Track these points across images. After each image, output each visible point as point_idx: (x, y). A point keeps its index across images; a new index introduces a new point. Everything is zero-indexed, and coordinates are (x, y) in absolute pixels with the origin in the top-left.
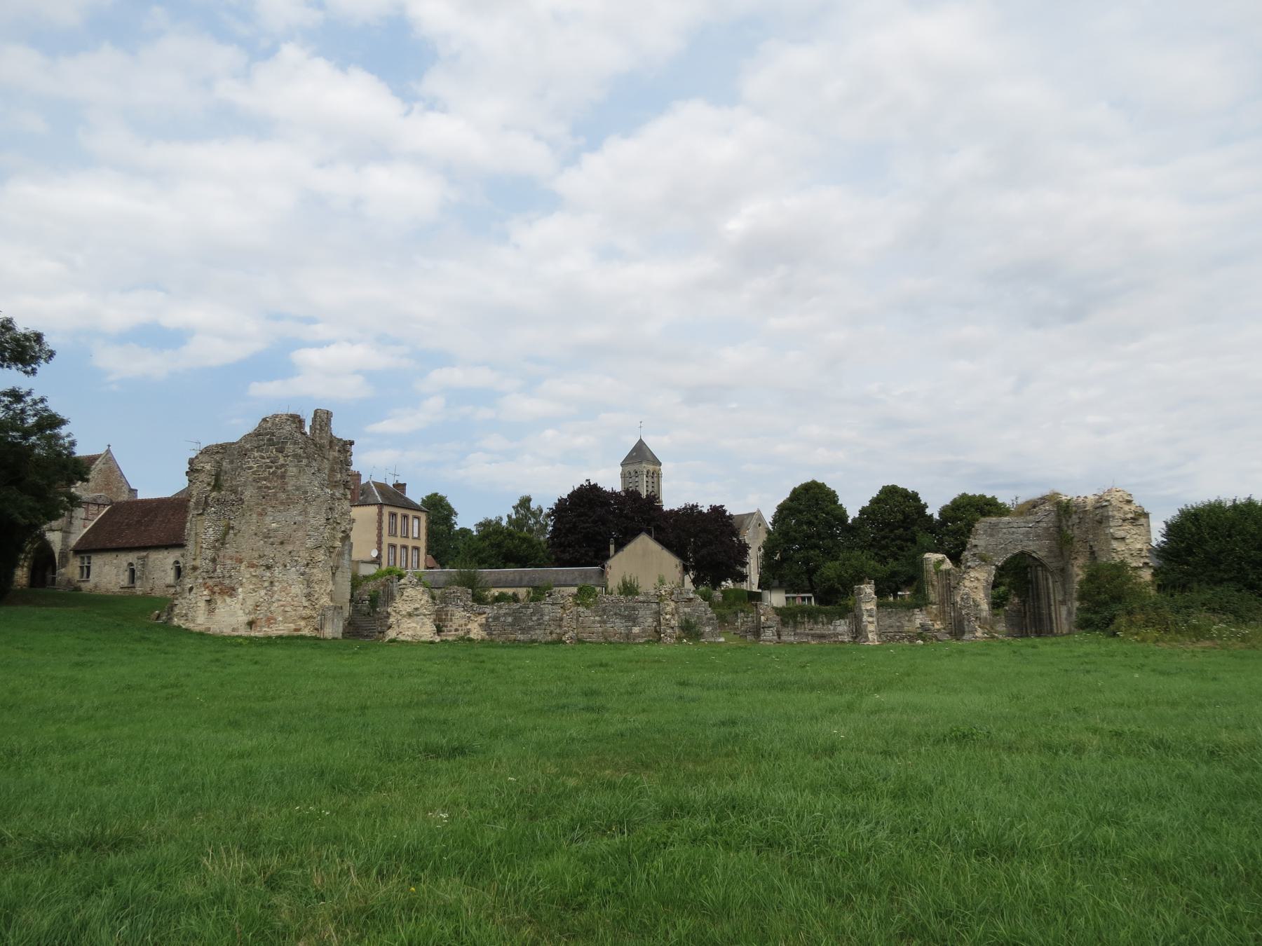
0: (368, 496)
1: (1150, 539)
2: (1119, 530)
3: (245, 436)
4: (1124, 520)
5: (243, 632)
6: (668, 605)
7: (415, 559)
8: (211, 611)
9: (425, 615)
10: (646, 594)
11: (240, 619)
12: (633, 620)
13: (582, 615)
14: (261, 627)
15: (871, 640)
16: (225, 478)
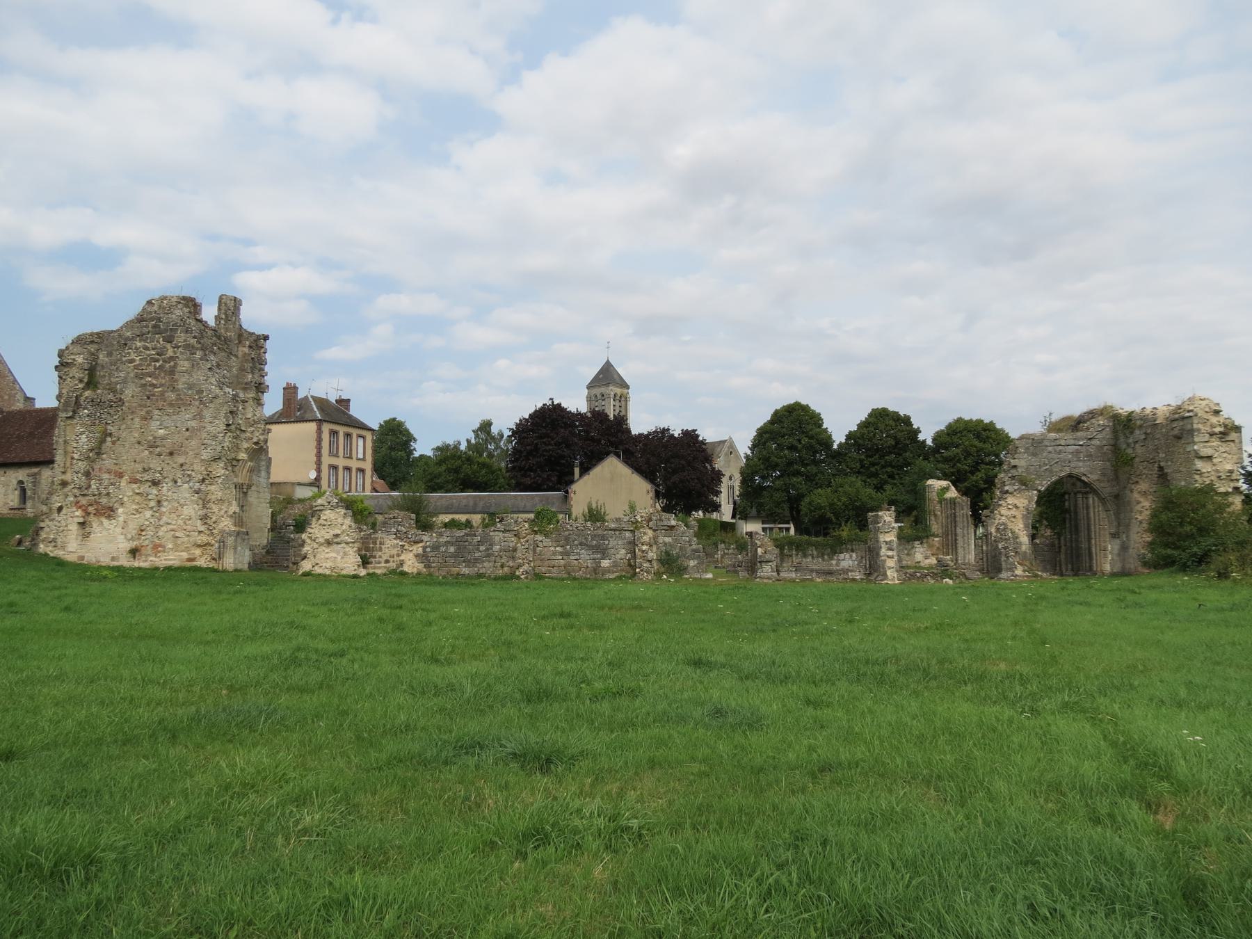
0: (305, 412)
1: (1242, 458)
2: (1205, 447)
3: (127, 323)
4: (1212, 435)
5: (125, 562)
6: (645, 533)
7: (360, 482)
8: (86, 536)
9: (347, 543)
10: (618, 520)
11: (121, 546)
12: (602, 551)
13: (540, 544)
14: (147, 555)
15: (890, 577)
16: (102, 374)
